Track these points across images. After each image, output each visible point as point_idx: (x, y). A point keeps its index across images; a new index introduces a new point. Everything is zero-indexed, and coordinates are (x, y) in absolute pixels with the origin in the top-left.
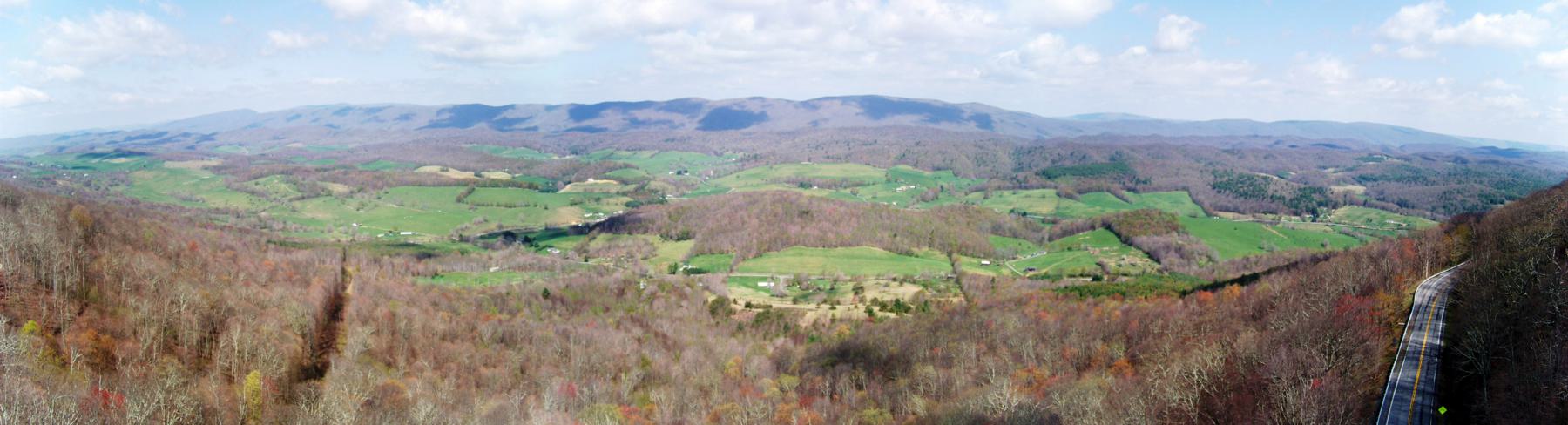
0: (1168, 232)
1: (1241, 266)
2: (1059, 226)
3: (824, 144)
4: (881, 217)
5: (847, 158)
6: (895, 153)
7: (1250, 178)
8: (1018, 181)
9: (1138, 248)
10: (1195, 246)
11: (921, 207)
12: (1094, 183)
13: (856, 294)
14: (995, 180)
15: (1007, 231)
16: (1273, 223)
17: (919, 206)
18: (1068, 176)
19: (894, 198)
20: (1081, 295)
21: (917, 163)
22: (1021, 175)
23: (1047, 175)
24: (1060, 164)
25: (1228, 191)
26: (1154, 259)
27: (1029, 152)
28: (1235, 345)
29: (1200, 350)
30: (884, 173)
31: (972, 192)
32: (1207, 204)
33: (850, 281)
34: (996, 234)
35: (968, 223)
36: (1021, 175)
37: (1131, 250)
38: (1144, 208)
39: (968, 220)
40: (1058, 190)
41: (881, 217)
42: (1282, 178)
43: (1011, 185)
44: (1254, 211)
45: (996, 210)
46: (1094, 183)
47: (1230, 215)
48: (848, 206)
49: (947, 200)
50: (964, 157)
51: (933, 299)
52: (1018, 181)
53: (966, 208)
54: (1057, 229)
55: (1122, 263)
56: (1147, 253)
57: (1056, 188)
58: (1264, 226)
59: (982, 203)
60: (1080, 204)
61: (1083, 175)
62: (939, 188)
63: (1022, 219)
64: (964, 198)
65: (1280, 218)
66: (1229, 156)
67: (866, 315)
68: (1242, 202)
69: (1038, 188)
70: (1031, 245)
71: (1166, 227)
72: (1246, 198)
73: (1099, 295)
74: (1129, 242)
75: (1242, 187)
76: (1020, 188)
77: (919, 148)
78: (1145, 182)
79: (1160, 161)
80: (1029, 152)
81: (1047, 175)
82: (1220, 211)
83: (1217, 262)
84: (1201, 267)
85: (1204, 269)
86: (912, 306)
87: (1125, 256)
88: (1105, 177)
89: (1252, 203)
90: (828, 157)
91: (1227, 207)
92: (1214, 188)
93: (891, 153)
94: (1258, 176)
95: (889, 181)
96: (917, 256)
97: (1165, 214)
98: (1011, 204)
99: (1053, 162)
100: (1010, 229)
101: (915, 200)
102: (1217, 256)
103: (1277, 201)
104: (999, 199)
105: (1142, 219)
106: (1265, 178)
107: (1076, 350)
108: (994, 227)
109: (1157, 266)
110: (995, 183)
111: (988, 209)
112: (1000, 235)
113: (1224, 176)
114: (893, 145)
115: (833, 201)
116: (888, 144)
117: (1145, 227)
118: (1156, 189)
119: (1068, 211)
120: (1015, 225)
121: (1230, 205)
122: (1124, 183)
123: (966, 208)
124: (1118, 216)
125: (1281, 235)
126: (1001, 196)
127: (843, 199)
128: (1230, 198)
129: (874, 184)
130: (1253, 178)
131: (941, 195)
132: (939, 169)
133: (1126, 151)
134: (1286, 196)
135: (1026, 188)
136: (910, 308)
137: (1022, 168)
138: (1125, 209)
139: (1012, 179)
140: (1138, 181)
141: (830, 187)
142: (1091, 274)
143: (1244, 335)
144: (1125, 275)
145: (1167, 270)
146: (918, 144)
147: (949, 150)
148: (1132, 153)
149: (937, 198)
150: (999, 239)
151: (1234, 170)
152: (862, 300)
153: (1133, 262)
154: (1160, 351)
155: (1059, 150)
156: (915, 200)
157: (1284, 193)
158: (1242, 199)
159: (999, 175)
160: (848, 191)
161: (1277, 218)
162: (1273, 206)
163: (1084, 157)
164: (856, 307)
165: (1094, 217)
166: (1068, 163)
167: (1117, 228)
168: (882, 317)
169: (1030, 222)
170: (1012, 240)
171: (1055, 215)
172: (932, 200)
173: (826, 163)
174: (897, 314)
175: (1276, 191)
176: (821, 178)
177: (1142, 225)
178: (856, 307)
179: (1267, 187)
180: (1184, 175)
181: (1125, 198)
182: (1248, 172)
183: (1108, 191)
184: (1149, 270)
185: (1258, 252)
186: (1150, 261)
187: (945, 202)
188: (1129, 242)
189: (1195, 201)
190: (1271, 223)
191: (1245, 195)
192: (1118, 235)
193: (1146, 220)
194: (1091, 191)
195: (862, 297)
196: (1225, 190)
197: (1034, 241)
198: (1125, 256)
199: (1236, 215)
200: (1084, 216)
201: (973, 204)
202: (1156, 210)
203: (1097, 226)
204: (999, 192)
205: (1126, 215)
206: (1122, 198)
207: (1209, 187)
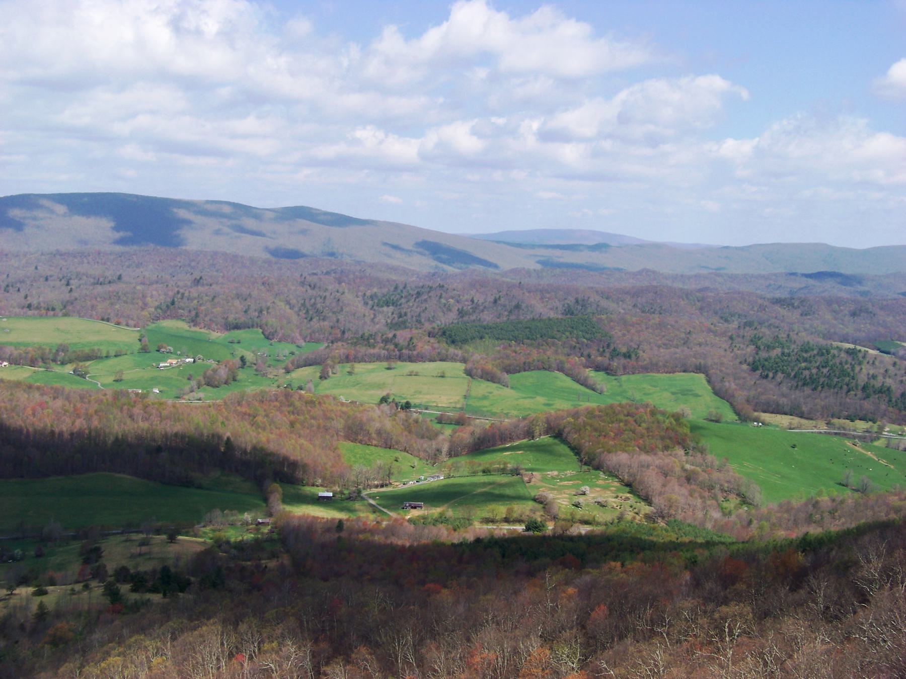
0: (666, 448)
1: (802, 515)
2: (470, 429)
3: (22, 282)
4: (131, 417)
5: (67, 309)
6: (156, 297)
7: (823, 352)
8: (396, 345)
9: (612, 473)
10: (716, 475)
11: (207, 395)
12: (534, 355)
13: (87, 561)
14: (340, 344)
15: (374, 435)
16: (867, 438)
17: (201, 395)
18: (488, 341)
19: (155, 381)
20: (503, 556)
21: (197, 315)
22: (403, 336)
23: (450, 336)
24: (473, 317)
25: (780, 376)
26: (639, 496)
27: (419, 294)
28: (789, 663)
29: (721, 666)
30: (137, 335)
31: (299, 367)
32: (740, 396)
33: (75, 538)
34: (354, 441)
35: (292, 424)
36: (403, 336)
37: (597, 477)
38: (624, 402)
39: (292, 417)
40: (469, 366)
41: (131, 417)
42: (888, 353)
43: (383, 352)
44: (829, 414)
45: (343, 399)
46: (534, 355)
47: (784, 420)
48: (68, 398)
49: (254, 383)
50: (282, 305)
51: (232, 565)
52: (396, 345)
53: (287, 396)
54: (465, 435)
55: (581, 499)
56: (628, 485)
57: (464, 360)
58: (848, 443)
59: (316, 386)
60: (507, 392)
61: (516, 339)
62: (237, 360)
63: (402, 415)
64: (285, 379)
65: (881, 428)
66: (782, 311)
67: (106, 601)
68: (809, 396)
69: (431, 360)
70: (416, 461)
71: (663, 438)
72: (814, 389)
73: (536, 558)
74: (595, 462)
75: (806, 368)
76: (401, 358)
77: (200, 288)
78: (627, 356)
79: (656, 319)
80: (419, 294)
81: (450, 336)
82: (765, 412)
83: (756, 507)
84: (726, 513)
85: (733, 518)
86: (192, 579)
87: (586, 488)
88: (554, 344)
89: (826, 398)
90: (29, 306)
91: (778, 405)
92: (754, 369)
93: (149, 299)
94: (840, 349)
95: (144, 350)
96: (200, 487)
97: (663, 413)
98: (380, 386)
99: (461, 313)
100: (379, 432)
101: (193, 383)
102: (759, 497)
103: (874, 398)
104: (349, 378)
105: (621, 421)
106: (849, 352)
107: (492, 656)
108: (349, 428)
109: (646, 509)
110: (340, 349)
111: (327, 396)
112: (361, 442)
113: (774, 348)
114: (151, 284)
115: (38, 388)
116: (143, 283)
117: (625, 436)
118: (646, 369)
119: (486, 403)
120: (388, 425)
121: (783, 401)
122: (589, 356)
123: (287, 396)
124: (576, 415)
125: (883, 462)
126: (350, 373)
127: (58, 385)
128: (784, 389)
129: (116, 356)
130: (828, 352)
131: (241, 375)
132: (237, 327)
133: (594, 298)
134: (893, 387)
135: (411, 359)
136: (189, 583)
137: (404, 322)
138: (592, 403)
139: (386, 341)
140: (615, 354)
141: (33, 363)
142: (524, 518)
143: (806, 648)
144: (586, 522)
145: (663, 517)
146: (197, 282)
147: (255, 293)
148: (604, 303)
149: (235, 380)
150: (359, 448)
151: (793, 336)
152: (99, 574)
153: (599, 500)
154: (647, 664)
155: (473, 292)
156: (193, 383)
157: (889, 382)
158: (807, 390)
159: (346, 336)
160: (69, 369)
161: (875, 429)
162: (868, 405)
163: (518, 307)
164: (86, 587)
165: (533, 415)
166: (488, 317)
167: (573, 437)
168: (136, 602)
169: (416, 421)
170: (381, 451)
171: (462, 409)
172: (226, 383)
173: (26, 317)
174: (165, 595)
175: (874, 377)
176: (17, 345)
177: (619, 433)
178: (86, 587)
179: (857, 368)
180: (700, 345)
181: (590, 382)
182: (822, 342)
183: (561, 369)
184: (629, 515)
185: (835, 492)
186: (632, 499)
187: (250, 386)
188: (595, 462)
189: (717, 393)
190: (863, 438)
191: (812, 383)
192: (576, 450)
193: (626, 423)
194: (529, 369)
195: (99, 567)
196: (776, 373)
197: (422, 454)
198: (586, 488)
199: (796, 420)
200: (515, 413)
201: (301, 388)
202: (647, 406)
203: (537, 432)
204: (347, 367)
205: (590, 413)
206: (584, 383)
207: (745, 367)
